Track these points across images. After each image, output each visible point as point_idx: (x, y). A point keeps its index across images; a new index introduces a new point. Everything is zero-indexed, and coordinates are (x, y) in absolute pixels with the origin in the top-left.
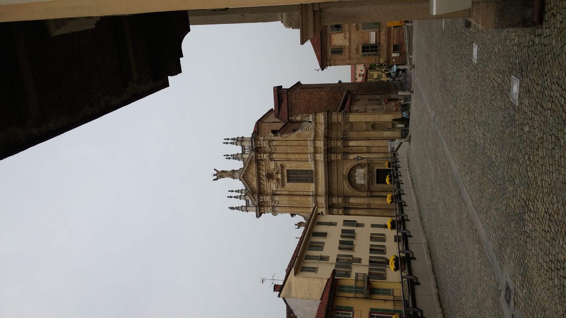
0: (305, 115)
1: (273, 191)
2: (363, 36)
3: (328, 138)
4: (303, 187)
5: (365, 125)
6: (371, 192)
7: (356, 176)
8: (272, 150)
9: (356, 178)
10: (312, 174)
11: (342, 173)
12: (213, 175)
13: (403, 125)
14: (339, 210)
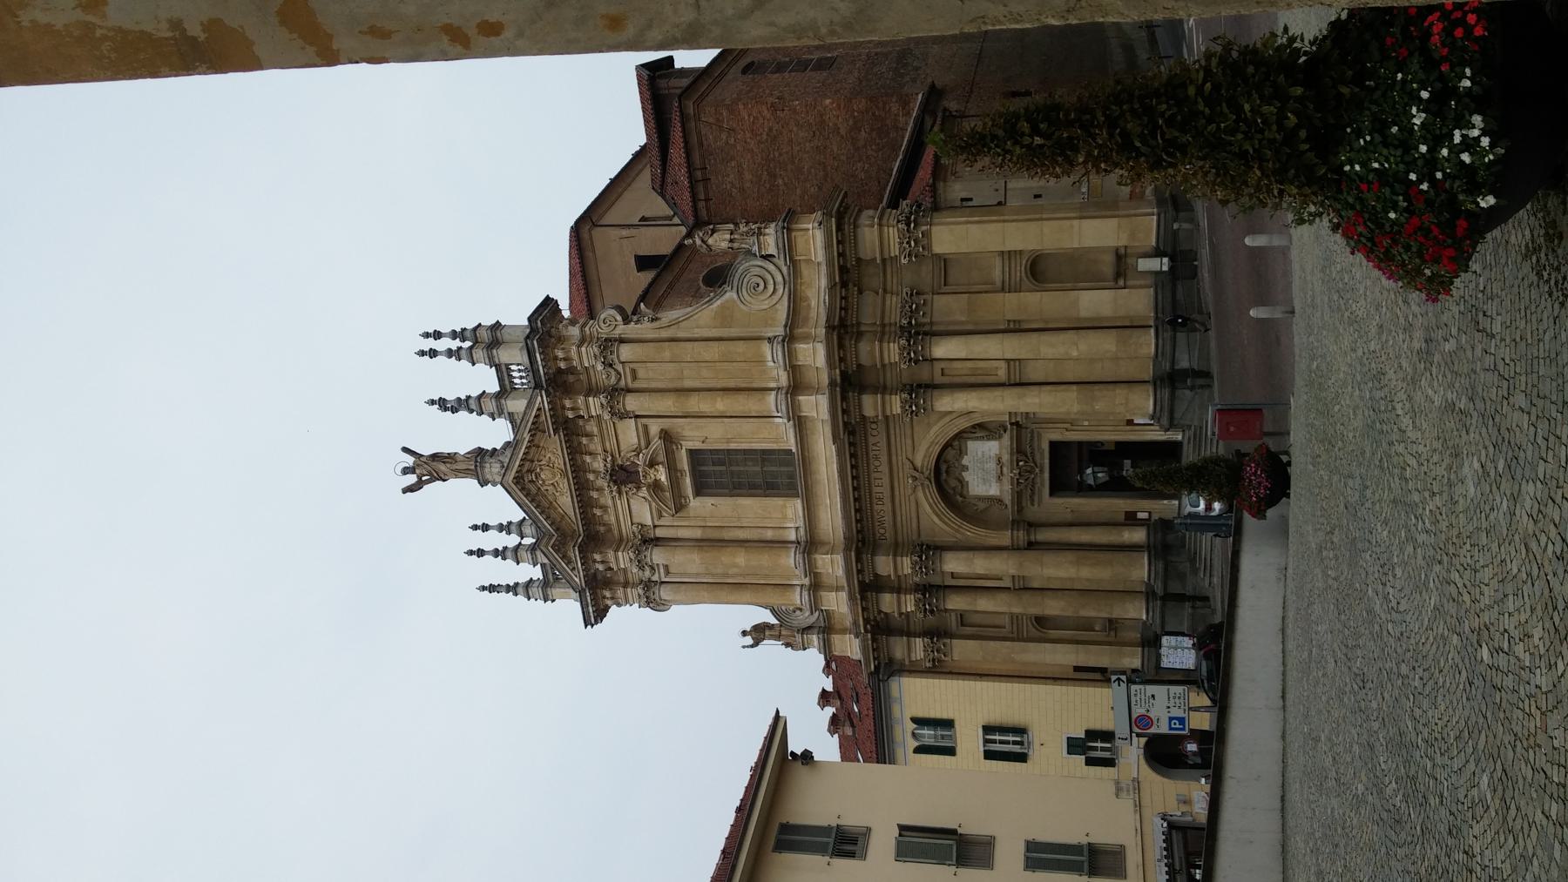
0: (745, 229)
3: (842, 330)
4: (760, 511)
5: (998, 262)
6: (1032, 525)
7: (965, 468)
8: (620, 379)
10: (790, 463)
12: (399, 470)
13: (1165, 260)
14: (903, 597)
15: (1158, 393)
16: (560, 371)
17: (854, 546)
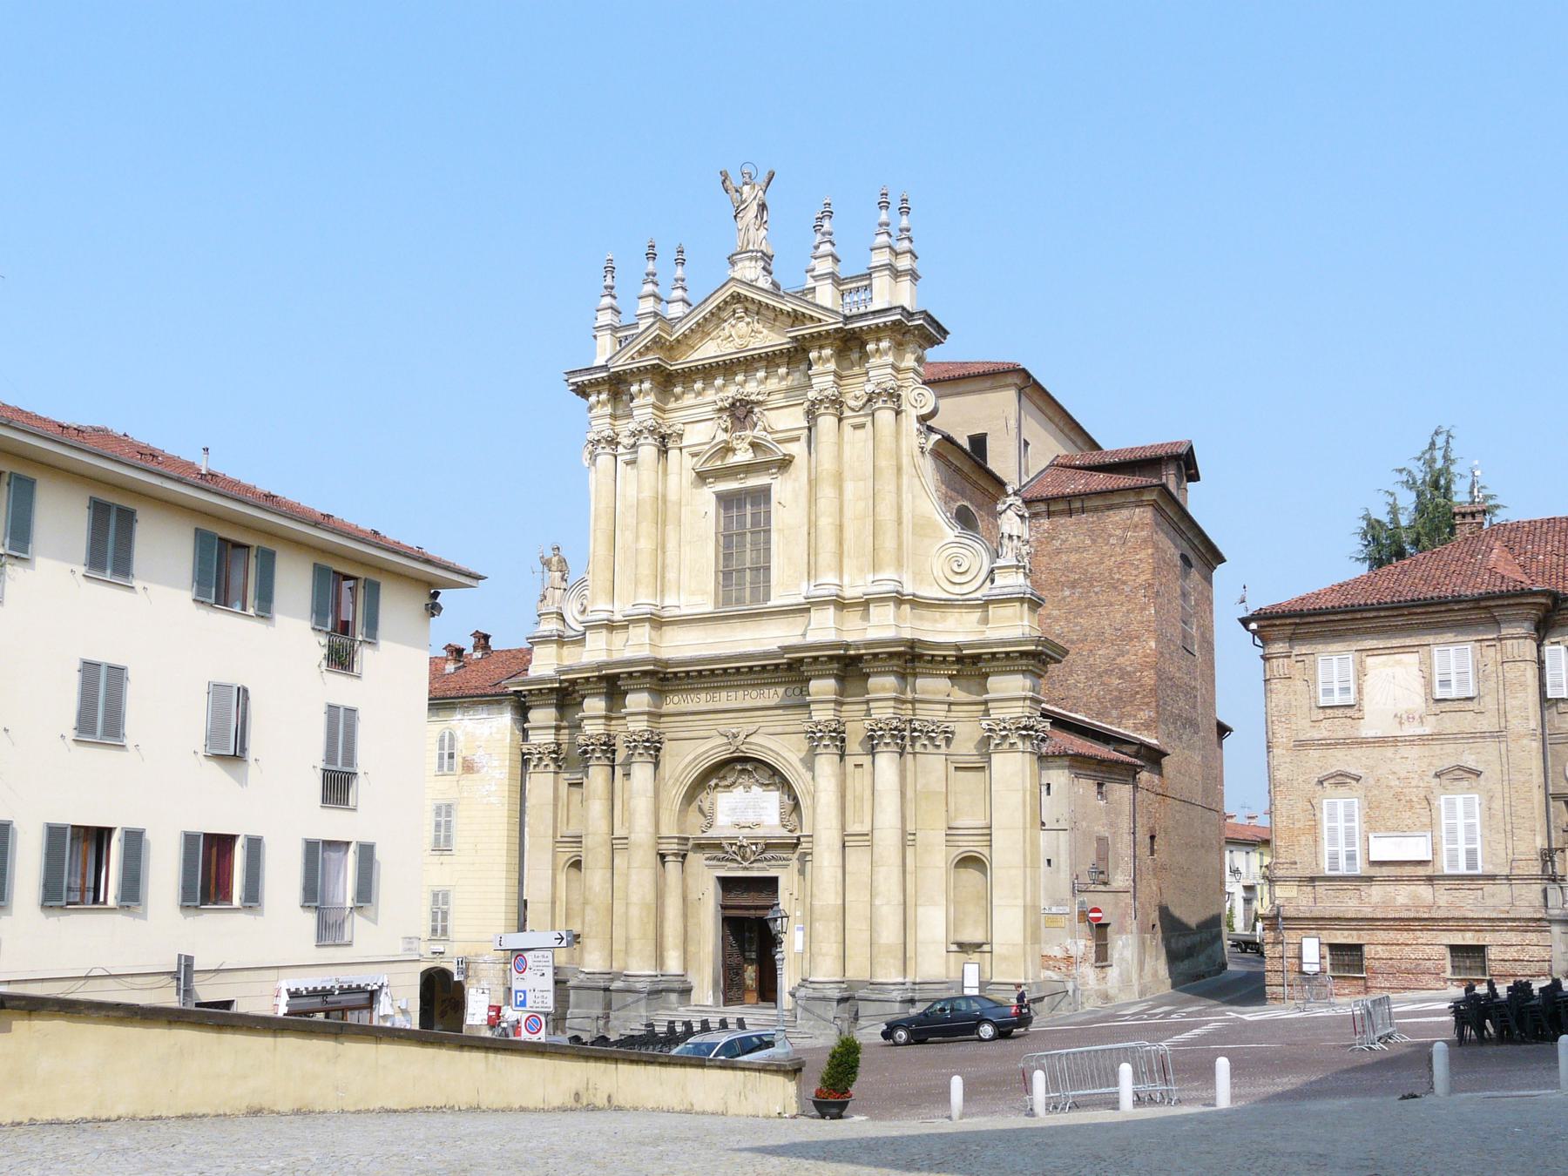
1: (681, 436)
2: (1411, 801)
8: (853, 410)
9: (738, 791)
10: (754, 599)
11: (755, 728)
13: (975, 992)
15: (832, 986)
16: (863, 344)
17: (659, 669)
